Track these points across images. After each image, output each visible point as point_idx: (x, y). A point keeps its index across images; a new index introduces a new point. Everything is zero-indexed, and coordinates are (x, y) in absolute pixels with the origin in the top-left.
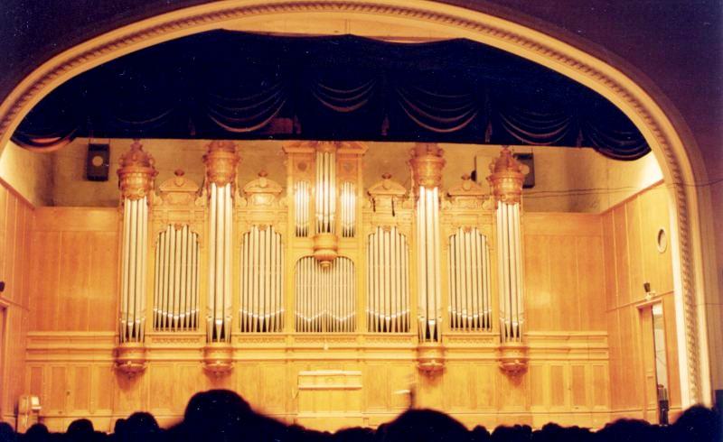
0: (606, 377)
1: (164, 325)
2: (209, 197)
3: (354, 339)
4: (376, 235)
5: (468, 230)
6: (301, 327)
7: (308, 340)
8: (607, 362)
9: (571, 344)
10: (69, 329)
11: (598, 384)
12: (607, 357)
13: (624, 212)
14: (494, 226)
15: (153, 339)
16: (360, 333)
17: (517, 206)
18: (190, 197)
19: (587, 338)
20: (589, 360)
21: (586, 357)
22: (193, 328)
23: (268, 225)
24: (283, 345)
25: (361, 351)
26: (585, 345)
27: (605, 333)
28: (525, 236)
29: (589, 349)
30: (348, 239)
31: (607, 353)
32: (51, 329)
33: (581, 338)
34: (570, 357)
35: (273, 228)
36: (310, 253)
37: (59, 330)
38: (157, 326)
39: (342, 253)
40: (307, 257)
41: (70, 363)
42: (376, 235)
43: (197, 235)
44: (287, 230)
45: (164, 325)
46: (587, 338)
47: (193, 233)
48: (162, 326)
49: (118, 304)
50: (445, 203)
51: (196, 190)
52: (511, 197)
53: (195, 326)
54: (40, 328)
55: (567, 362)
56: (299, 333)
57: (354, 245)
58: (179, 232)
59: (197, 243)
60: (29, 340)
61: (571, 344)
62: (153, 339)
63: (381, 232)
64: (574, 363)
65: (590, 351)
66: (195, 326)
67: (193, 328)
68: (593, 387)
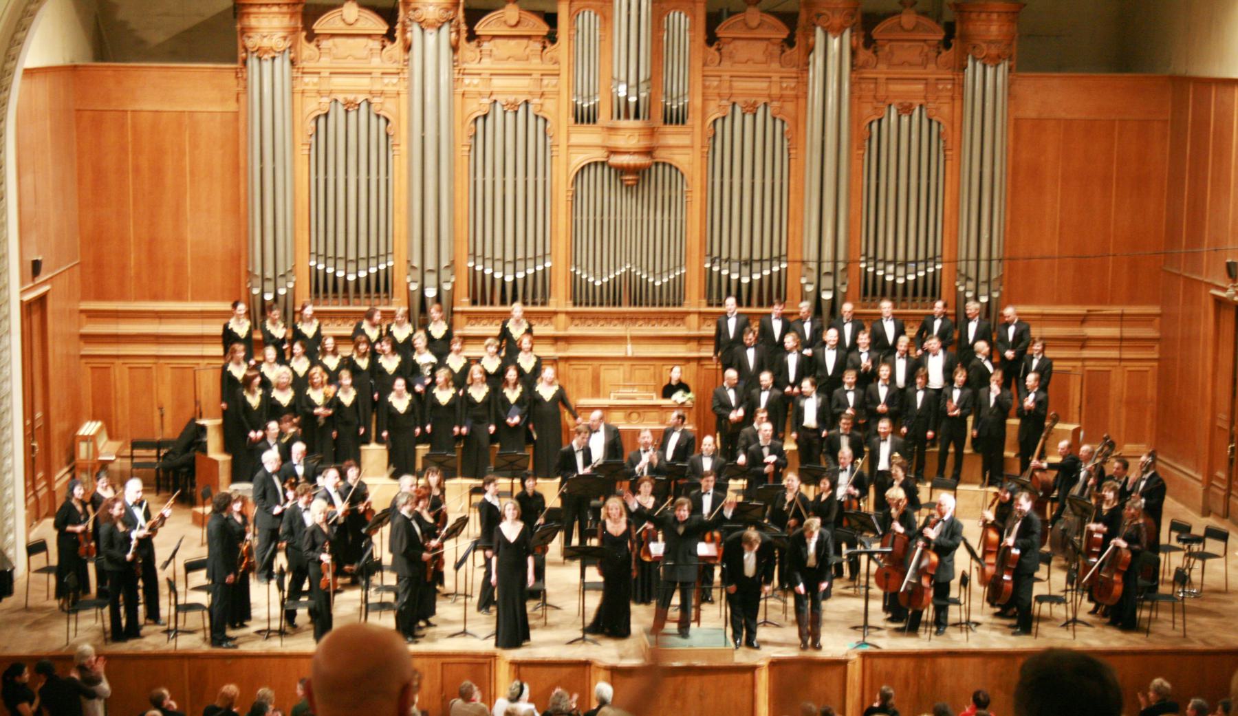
0: (1151, 391)
1: (879, 292)
2: (408, 48)
3: (681, 317)
4: (728, 121)
5: (906, 109)
6: (580, 293)
7: (596, 318)
8: (1155, 364)
9: (1091, 331)
10: (155, 297)
11: (1134, 403)
12: (1156, 356)
13: (1110, 71)
14: (801, 101)
15: (469, 319)
16: (559, 309)
17: (1003, 68)
18: (926, 49)
19: (1122, 319)
20: (1121, 360)
21: (1114, 354)
22: (910, 297)
23: (761, 101)
24: (681, 331)
25: (561, 345)
26: (1113, 331)
27: (1155, 310)
28: (1016, 119)
29: (1122, 339)
30: (585, 127)
31: (1157, 347)
32: (122, 297)
33: (1108, 319)
34: (1086, 353)
35: (531, 107)
36: (599, 155)
37: (137, 299)
38: (317, 290)
39: (661, 155)
40: (596, 163)
41: (162, 361)
42: (728, 121)
43: (387, 121)
44: (558, 109)
45: (879, 292)
46: (1122, 319)
47: (378, 116)
48: (326, 290)
49: (243, 253)
50: (864, 55)
51: (785, 36)
52: (994, 51)
53: (386, 290)
54: (100, 297)
55: (1079, 364)
56: (578, 309)
57: (685, 140)
58: (352, 115)
59: (387, 135)
60: (83, 316)
61: (1091, 331)
62: (469, 319)
63: (738, 110)
64: (1090, 365)
65: (1125, 344)
66: (386, 290)
67: (383, 295)
68: (1124, 411)
